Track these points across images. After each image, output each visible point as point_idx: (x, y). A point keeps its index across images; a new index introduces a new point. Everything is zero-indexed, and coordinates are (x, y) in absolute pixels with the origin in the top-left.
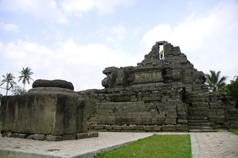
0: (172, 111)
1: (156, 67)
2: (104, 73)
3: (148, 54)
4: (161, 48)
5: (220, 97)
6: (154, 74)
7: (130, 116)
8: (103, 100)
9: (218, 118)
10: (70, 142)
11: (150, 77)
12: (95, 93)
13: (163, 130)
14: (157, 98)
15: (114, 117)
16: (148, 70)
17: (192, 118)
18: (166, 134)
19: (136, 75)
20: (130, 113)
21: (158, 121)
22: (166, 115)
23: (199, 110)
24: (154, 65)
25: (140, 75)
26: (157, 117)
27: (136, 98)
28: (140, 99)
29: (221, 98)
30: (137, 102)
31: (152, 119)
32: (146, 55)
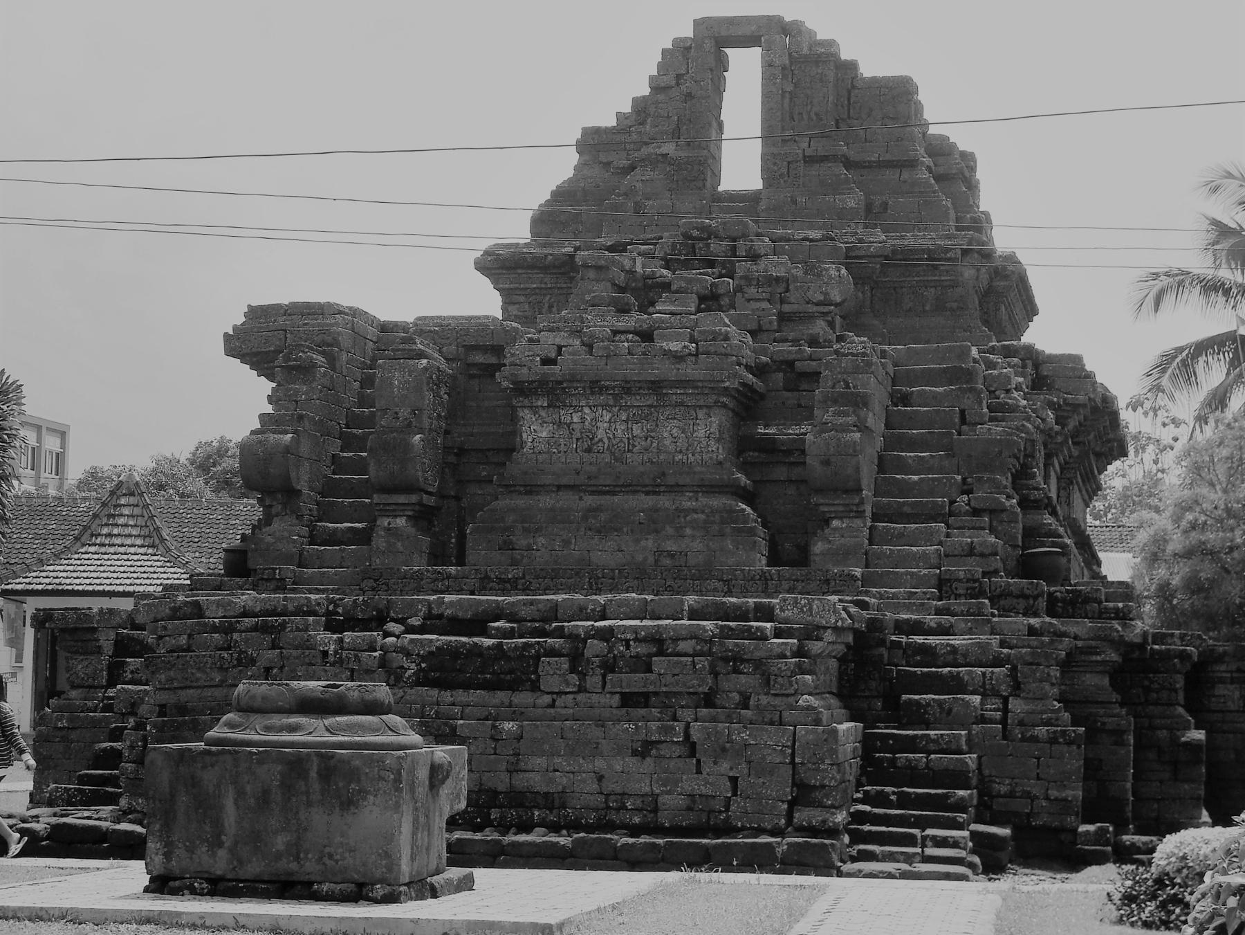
0: (769, 759)
2: (244, 357)
3: (611, 122)
4: (745, 74)
5: (1099, 658)
6: (670, 431)
9: (1047, 798)
13: (609, 615)
18: (755, 149)
20: (540, 762)
21: (689, 809)
22: (734, 780)
23: (932, 747)
25: (559, 424)
26: (688, 789)
27: (573, 670)
28: (593, 681)
29: (1103, 662)
30: (580, 697)
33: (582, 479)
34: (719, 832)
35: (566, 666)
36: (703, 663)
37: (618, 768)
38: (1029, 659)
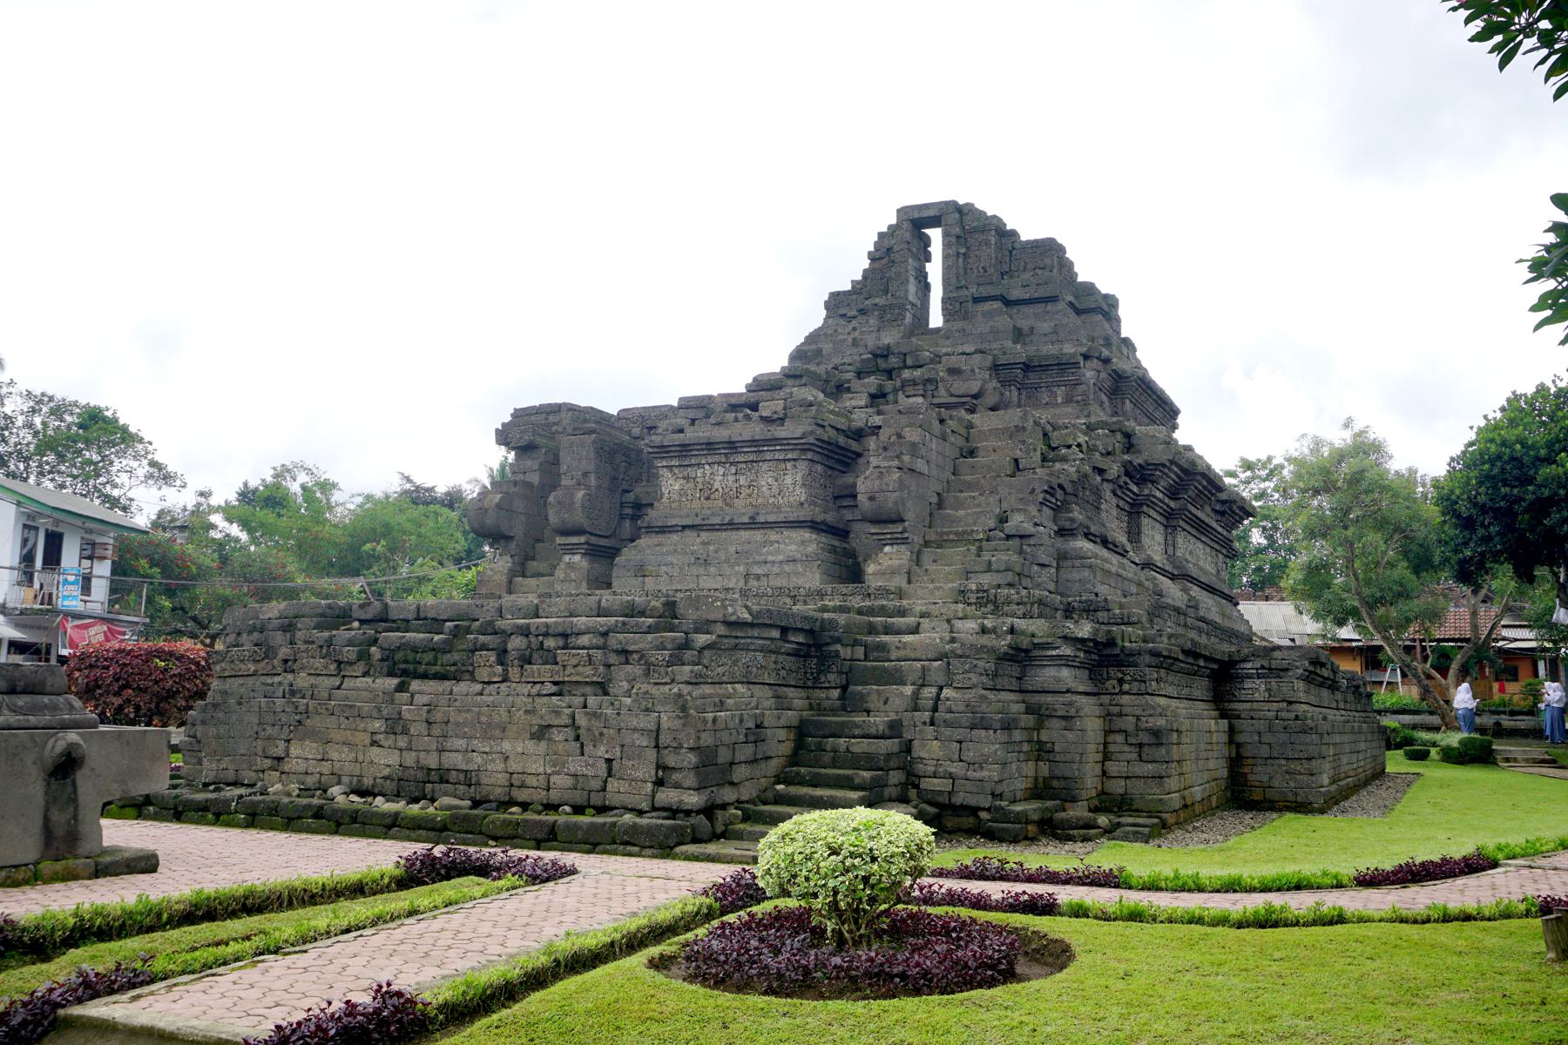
1: (781, 432)
3: (849, 287)
7: (459, 756)
8: (350, 663)
10: (477, 891)
11: (745, 491)
12: (319, 627)
14: (588, 671)
15: (393, 759)
16: (732, 446)
17: (803, 777)
19: (665, 473)
20: (461, 743)
22: (609, 761)
24: (767, 420)
25: (687, 478)
26: (573, 770)
30: (503, 686)
31: (553, 779)
32: (838, 293)
33: (698, 521)
34: (602, 810)
35: (493, 659)
36: (598, 654)
37: (520, 750)
38: (959, 652)
